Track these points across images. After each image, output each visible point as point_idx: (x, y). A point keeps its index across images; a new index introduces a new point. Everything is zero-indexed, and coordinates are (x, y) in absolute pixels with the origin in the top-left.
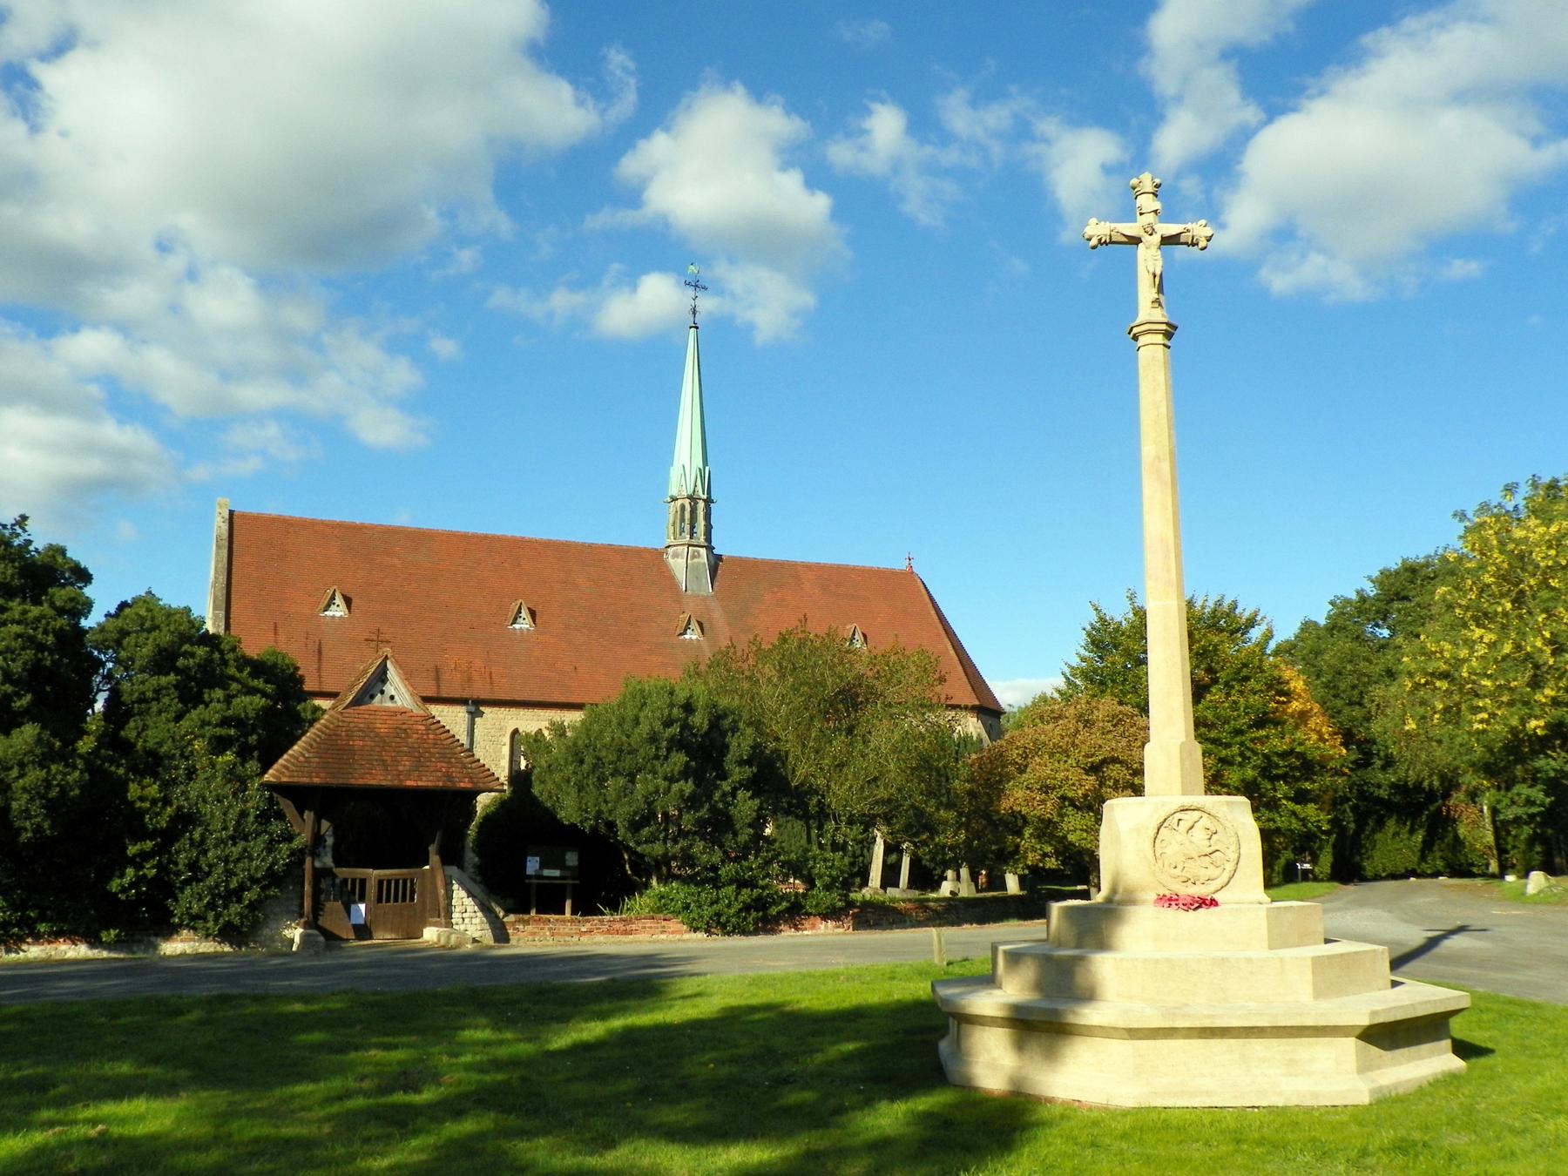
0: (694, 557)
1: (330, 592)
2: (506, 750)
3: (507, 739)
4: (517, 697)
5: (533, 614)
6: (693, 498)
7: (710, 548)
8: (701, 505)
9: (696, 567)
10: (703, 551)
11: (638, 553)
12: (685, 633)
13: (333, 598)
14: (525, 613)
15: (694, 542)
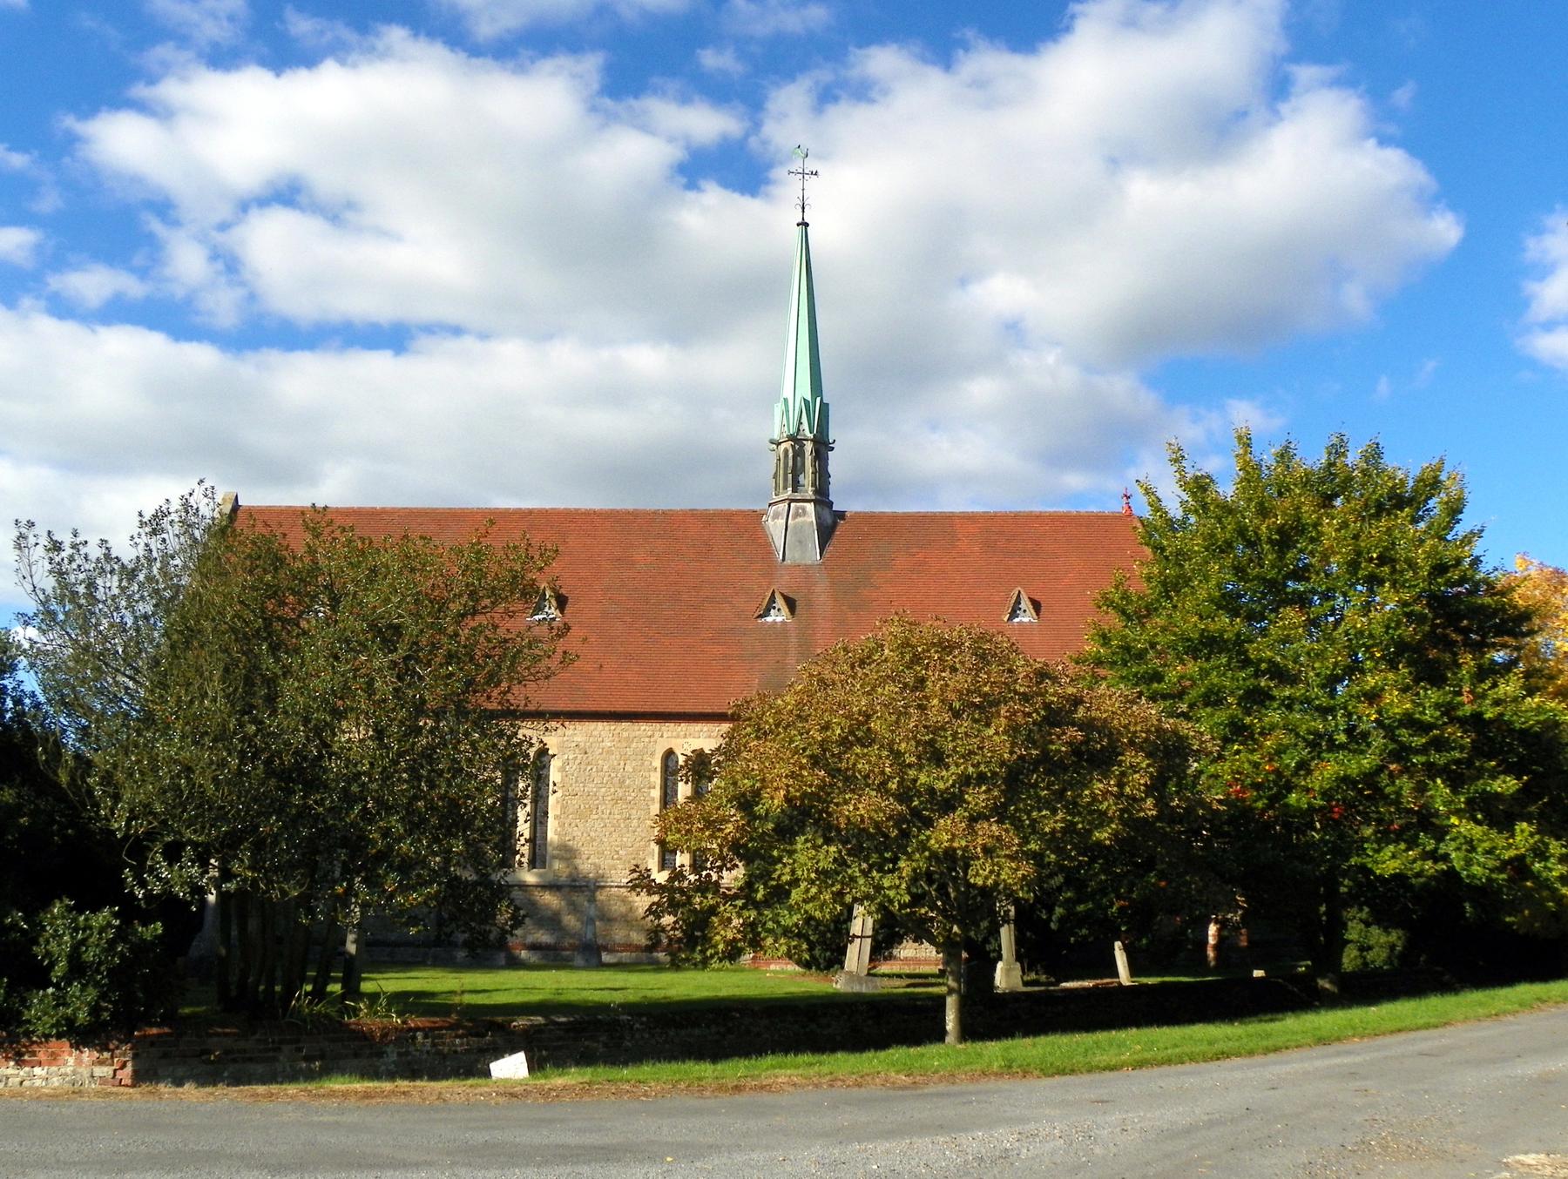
0: (797, 515)
1: (769, 594)
2: (656, 778)
3: (657, 763)
4: (688, 709)
5: (1037, 605)
6: (795, 439)
7: (822, 497)
8: (809, 446)
9: (800, 529)
10: (810, 507)
11: (728, 517)
12: (767, 613)
13: (1018, 602)
14: (1025, 604)
15: (798, 496)
